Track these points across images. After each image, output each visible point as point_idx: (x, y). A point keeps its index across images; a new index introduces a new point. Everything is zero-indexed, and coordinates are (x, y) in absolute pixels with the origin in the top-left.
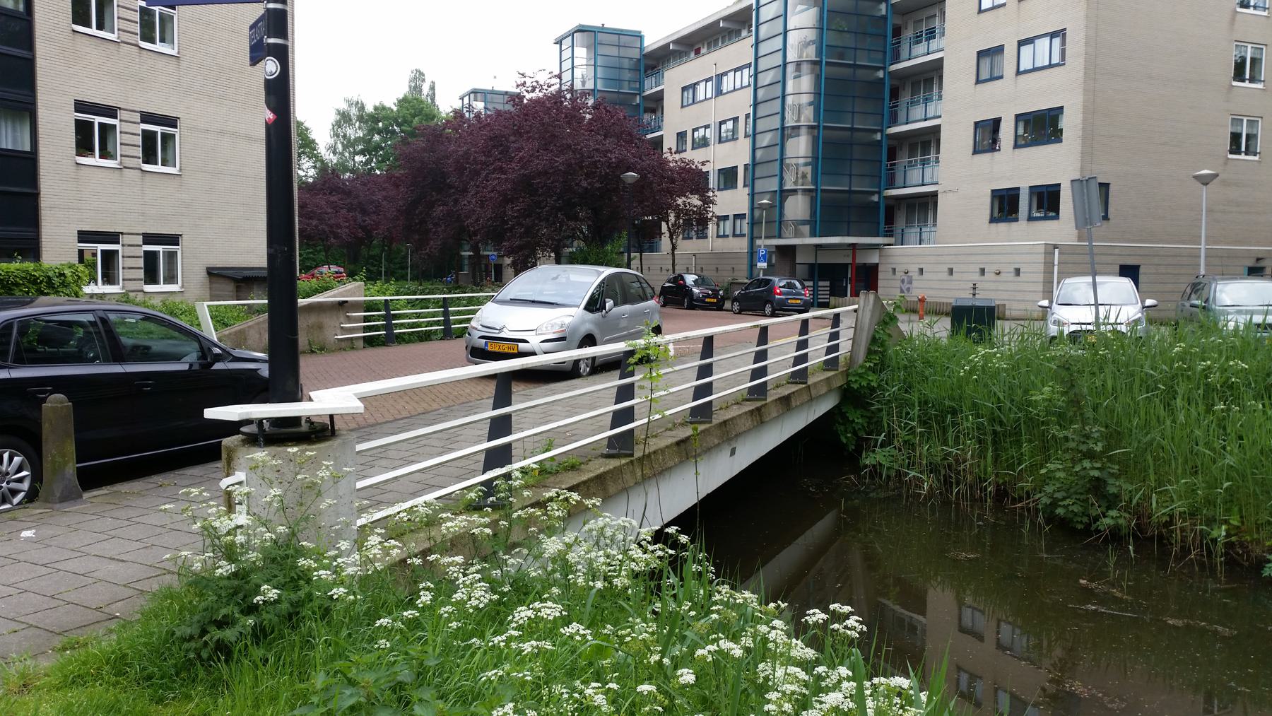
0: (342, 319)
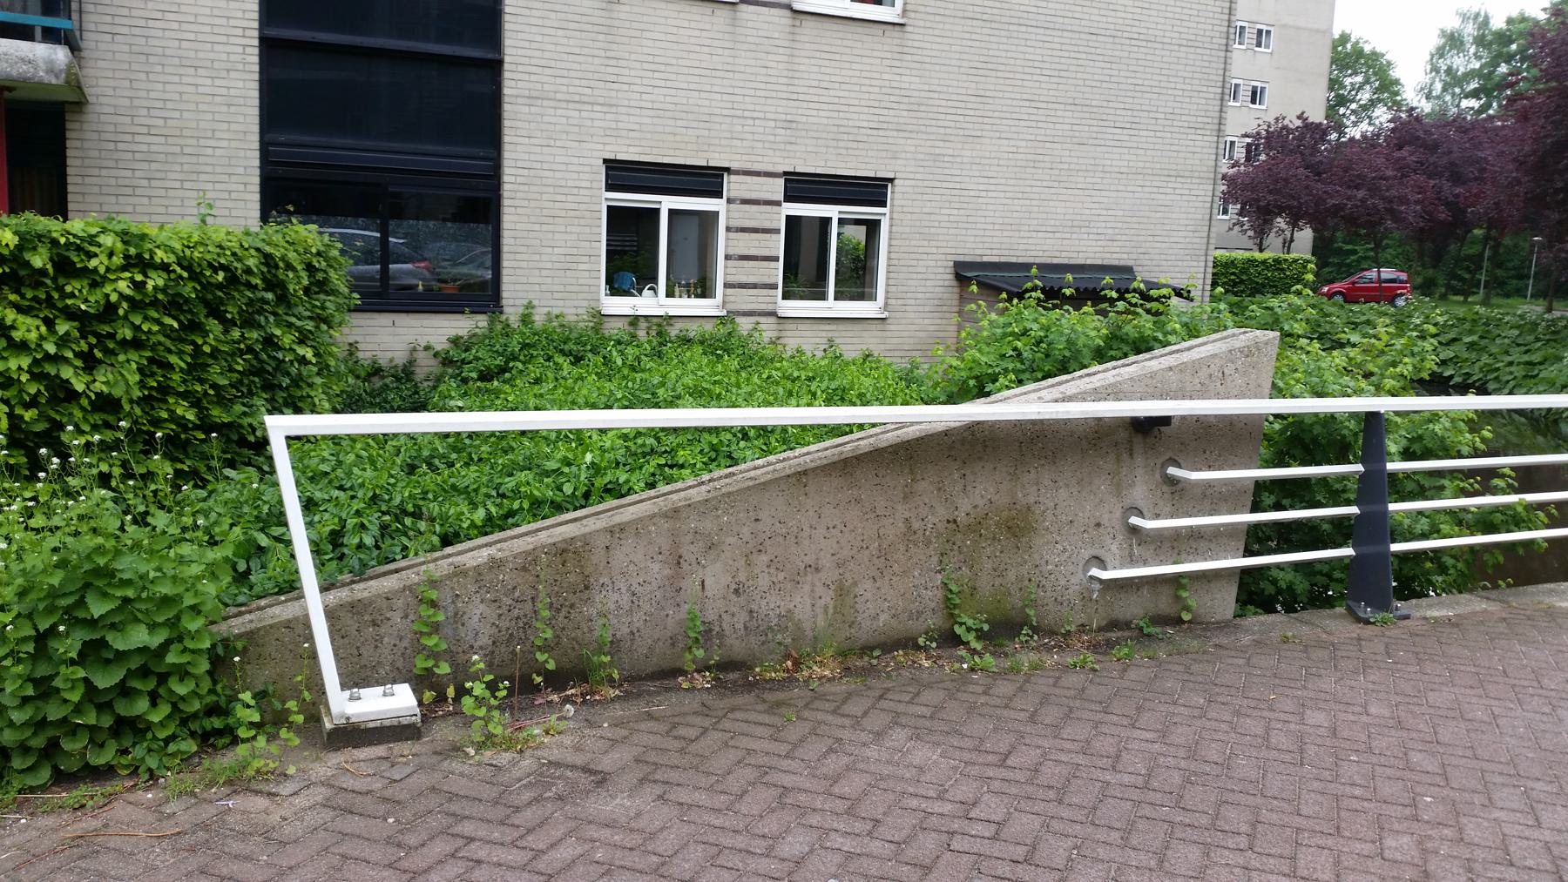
0: (1139, 493)
